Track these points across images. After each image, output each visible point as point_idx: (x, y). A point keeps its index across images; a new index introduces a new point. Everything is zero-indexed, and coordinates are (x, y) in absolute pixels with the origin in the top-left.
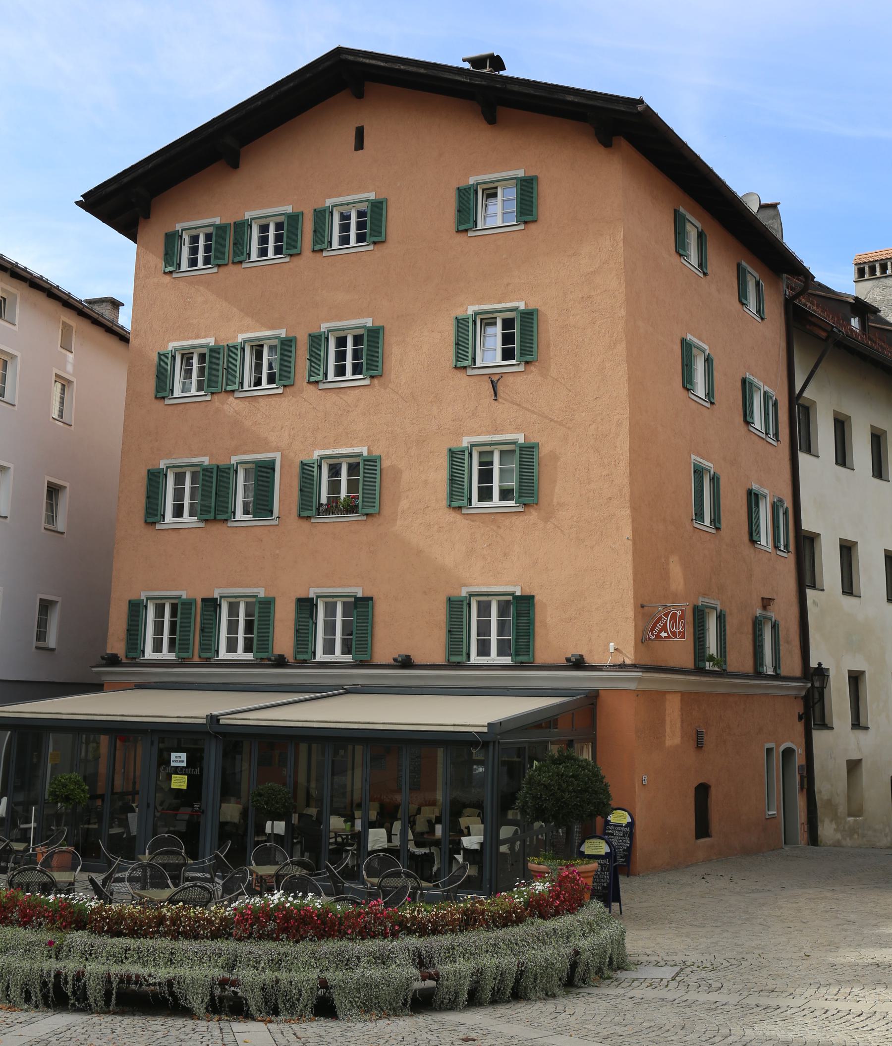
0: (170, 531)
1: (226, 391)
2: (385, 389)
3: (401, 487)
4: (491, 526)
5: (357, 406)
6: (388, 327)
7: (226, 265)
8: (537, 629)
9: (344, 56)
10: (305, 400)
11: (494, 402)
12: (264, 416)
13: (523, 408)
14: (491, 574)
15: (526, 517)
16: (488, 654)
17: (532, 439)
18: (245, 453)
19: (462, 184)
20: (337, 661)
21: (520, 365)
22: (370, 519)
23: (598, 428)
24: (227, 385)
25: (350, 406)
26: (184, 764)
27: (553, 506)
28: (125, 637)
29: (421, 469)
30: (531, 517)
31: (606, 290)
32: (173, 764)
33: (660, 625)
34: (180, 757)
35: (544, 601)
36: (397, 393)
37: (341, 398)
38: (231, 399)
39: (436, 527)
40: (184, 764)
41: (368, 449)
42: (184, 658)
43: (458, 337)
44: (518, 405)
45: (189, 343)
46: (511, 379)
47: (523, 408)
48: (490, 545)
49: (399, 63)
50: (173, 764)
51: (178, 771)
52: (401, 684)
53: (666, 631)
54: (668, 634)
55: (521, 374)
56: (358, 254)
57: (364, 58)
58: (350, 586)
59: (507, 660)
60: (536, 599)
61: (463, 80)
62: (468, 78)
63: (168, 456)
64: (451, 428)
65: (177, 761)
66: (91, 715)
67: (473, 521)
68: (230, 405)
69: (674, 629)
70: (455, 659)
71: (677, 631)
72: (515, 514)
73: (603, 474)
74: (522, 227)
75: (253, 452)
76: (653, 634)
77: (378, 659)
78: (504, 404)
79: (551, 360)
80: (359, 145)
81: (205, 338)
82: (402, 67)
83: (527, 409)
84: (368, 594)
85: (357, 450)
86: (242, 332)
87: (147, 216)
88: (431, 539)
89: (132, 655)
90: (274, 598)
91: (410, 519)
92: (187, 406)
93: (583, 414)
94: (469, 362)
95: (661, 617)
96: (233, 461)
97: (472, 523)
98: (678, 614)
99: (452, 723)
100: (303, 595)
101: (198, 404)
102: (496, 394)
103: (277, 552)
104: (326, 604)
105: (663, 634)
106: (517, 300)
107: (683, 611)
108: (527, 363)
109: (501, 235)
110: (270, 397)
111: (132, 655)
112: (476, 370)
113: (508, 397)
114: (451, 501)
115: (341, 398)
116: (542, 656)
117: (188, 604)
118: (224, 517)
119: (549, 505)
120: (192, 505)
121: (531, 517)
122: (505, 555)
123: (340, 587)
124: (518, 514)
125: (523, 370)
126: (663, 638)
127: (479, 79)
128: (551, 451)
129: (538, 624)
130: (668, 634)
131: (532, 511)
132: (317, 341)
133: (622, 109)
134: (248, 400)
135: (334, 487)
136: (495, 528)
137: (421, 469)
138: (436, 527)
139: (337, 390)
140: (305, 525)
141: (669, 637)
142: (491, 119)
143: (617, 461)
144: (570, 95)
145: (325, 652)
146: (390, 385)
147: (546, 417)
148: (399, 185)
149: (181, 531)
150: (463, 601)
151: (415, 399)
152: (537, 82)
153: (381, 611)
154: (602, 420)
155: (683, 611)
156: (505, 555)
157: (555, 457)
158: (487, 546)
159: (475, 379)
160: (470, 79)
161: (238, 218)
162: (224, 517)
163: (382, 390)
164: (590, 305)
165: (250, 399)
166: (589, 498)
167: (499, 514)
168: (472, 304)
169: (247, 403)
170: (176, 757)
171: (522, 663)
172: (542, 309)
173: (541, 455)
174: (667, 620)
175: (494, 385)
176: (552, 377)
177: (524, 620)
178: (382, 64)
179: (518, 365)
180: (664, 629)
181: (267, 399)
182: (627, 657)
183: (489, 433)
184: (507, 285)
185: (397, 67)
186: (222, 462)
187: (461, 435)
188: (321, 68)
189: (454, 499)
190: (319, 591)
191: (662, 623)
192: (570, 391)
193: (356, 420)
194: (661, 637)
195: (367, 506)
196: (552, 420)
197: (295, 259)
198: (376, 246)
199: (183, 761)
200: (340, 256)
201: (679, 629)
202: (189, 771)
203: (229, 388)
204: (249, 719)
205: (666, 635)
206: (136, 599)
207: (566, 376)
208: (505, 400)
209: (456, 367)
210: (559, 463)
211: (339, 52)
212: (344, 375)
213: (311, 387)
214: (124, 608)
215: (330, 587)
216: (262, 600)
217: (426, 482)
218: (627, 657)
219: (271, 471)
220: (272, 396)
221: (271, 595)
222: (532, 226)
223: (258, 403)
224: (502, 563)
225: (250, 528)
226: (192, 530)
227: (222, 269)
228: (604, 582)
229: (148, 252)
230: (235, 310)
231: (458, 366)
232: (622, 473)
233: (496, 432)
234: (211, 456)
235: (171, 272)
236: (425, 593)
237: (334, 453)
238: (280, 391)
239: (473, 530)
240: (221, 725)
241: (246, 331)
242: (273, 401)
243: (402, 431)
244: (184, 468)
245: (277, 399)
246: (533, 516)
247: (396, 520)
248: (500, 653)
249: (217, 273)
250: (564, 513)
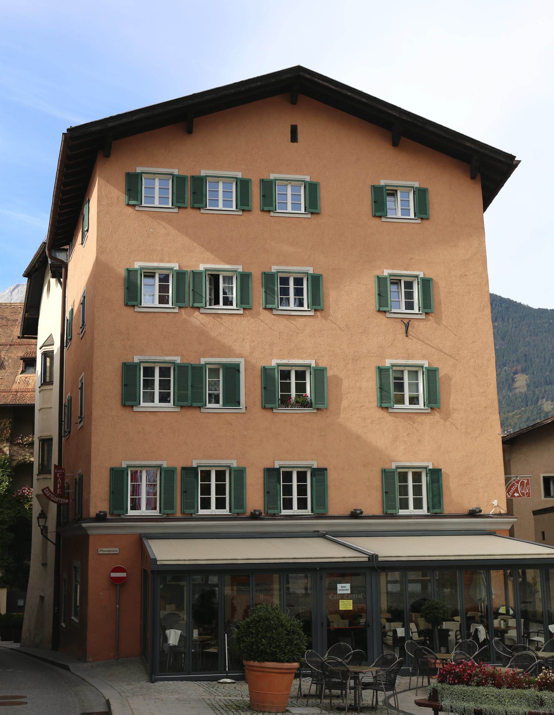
0: (147, 413)
1: (193, 307)
2: (326, 320)
3: (342, 391)
4: (409, 422)
5: (304, 330)
6: (325, 276)
7: (186, 208)
8: (444, 491)
9: (302, 73)
10: (262, 321)
11: (405, 337)
12: (228, 330)
13: (425, 343)
14: (411, 454)
15: (432, 417)
17: (433, 365)
18: (212, 356)
20: (299, 514)
21: (422, 315)
22: (319, 412)
23: (475, 361)
24: (194, 302)
25: (299, 329)
26: (349, 592)
27: (450, 410)
28: (108, 497)
29: (357, 379)
30: (435, 417)
31: (476, 273)
32: (339, 592)
33: (513, 489)
34: (345, 587)
35: (448, 472)
36: (335, 324)
37: (291, 323)
38: (197, 313)
39: (370, 420)
40: (349, 592)
41: (315, 361)
42: (168, 514)
43: (379, 290)
44: (423, 341)
45: (155, 264)
46: (416, 323)
47: (425, 343)
48: (408, 434)
49: (346, 90)
50: (339, 592)
51: (344, 597)
52: (150, 532)
53: (518, 493)
54: (519, 494)
55: (423, 320)
56: (298, 219)
57: (318, 79)
58: (307, 460)
60: (442, 471)
61: (394, 114)
62: (398, 113)
63: (141, 353)
64: (377, 352)
65: (343, 590)
66: (265, 559)
67: (396, 417)
68: (196, 318)
69: (523, 491)
70: (390, 511)
71: (525, 492)
72: (425, 414)
73: (481, 391)
74: (176, 210)
75: (219, 356)
77: (332, 512)
78: (412, 339)
79: (443, 314)
80: (294, 138)
81: (169, 262)
82: (349, 94)
83: (428, 345)
84: (322, 466)
85: (307, 362)
86: (203, 263)
87: (107, 155)
88: (366, 428)
89: (116, 512)
90: (245, 468)
91: (350, 414)
92: (156, 315)
93: (465, 352)
94: (203, 305)
95: (514, 484)
97: (396, 419)
98: (525, 482)
99: (342, 556)
100: (270, 466)
101: (166, 314)
102: (406, 333)
103: (245, 433)
105: (516, 494)
106: (418, 270)
107: (528, 480)
108: (426, 313)
109: (404, 224)
110: (231, 316)
111: (116, 512)
113: (415, 335)
114: (382, 403)
115: (291, 323)
116: (447, 509)
118: (199, 404)
119: (447, 409)
121: (435, 417)
122: (419, 441)
123: (299, 460)
124: (427, 414)
125: (424, 318)
127: (406, 116)
128: (446, 374)
129: (444, 488)
130: (519, 494)
131: (436, 413)
132: (268, 278)
133: (502, 159)
134: (212, 315)
135: (301, 388)
136: (411, 423)
137: (357, 379)
138: (370, 420)
139: (288, 317)
140: (268, 414)
141: (520, 496)
142: (395, 144)
143: (489, 384)
144: (469, 142)
145: (415, 508)
146: (329, 318)
147: (441, 351)
148: (327, 174)
149: (158, 414)
150: (394, 472)
151: (349, 330)
152: (442, 126)
153: (332, 477)
154: (478, 356)
155: (528, 480)
156: (419, 441)
157: (448, 378)
158: (407, 435)
159: (391, 321)
160: (399, 115)
161: (195, 174)
162: (199, 404)
163: (324, 321)
164: (466, 280)
165: (214, 315)
166: (472, 406)
167: (413, 414)
168: (387, 268)
169: (212, 319)
170: (342, 587)
171: (436, 513)
172: (435, 278)
173: (440, 376)
174: (518, 486)
175: (407, 326)
176: (443, 325)
177: (436, 485)
178: (333, 87)
180: (516, 491)
181: (229, 317)
182: (502, 509)
183: (404, 358)
184: (411, 259)
185: (345, 93)
186: (192, 360)
187: (385, 358)
188: (283, 78)
189: (383, 401)
191: (515, 487)
192: (456, 335)
193: (304, 340)
194: (515, 496)
195: (319, 402)
196: (445, 353)
197: (246, 214)
198: (313, 216)
199: (348, 590)
200: (284, 218)
201: (526, 491)
202: (355, 596)
203: (196, 305)
204: (402, 557)
205: (518, 495)
206: (117, 466)
207: (453, 325)
208: (413, 337)
209: (379, 311)
210: (452, 382)
211: (299, 69)
212: (413, 309)
213: (266, 312)
214: (106, 475)
215: (290, 460)
216: (236, 469)
217: (360, 388)
218: (502, 509)
219: (237, 372)
220: (234, 315)
221: (242, 465)
222: (425, 222)
223: (222, 319)
224: (418, 447)
226: (168, 413)
227: (181, 210)
228: (485, 461)
229: (109, 185)
230: (195, 244)
231: (381, 310)
232: (493, 391)
233: (409, 358)
234: (182, 356)
235: (134, 206)
236: (364, 466)
237: (288, 362)
238: (241, 312)
239: (396, 424)
240: (379, 561)
241: (207, 262)
242: (235, 319)
243: (341, 351)
245: (238, 318)
246: (437, 416)
247: (340, 414)
249: (177, 213)
250: (457, 415)
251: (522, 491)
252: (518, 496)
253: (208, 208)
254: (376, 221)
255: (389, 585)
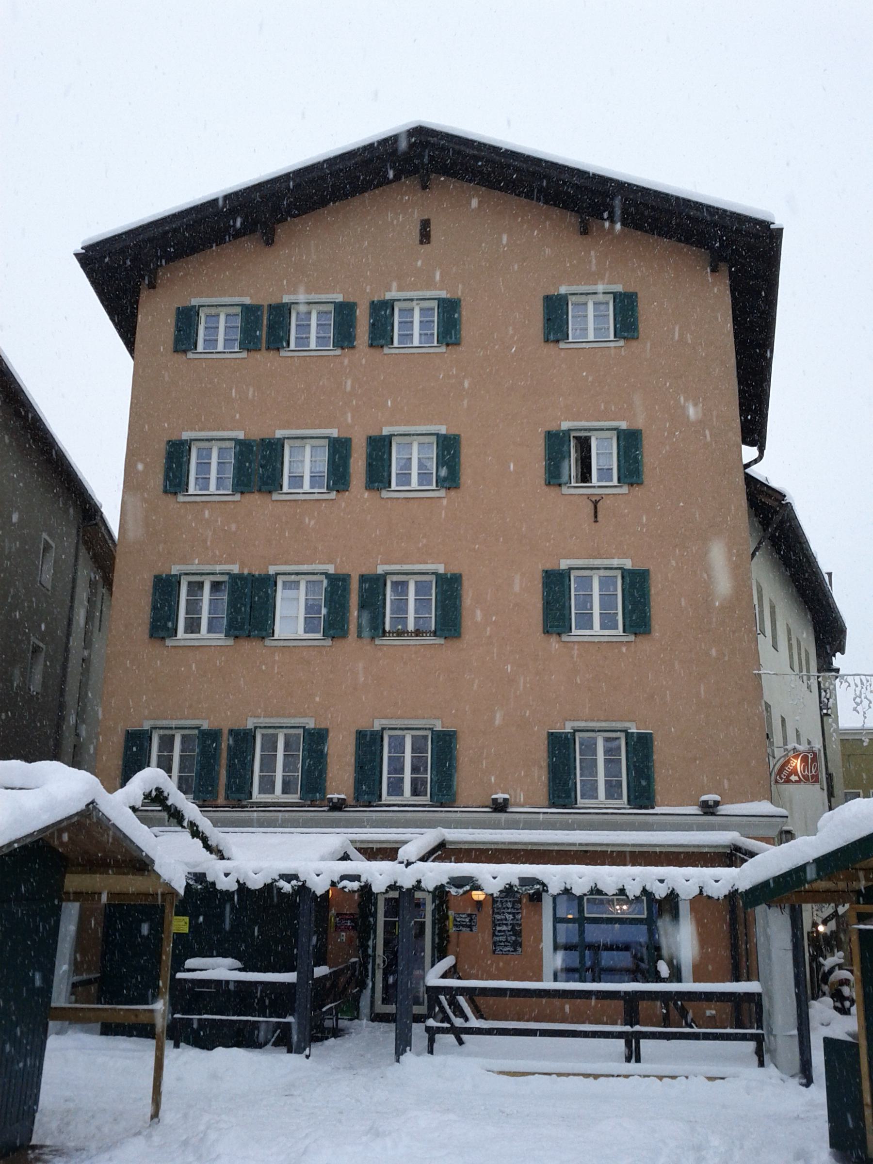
16: (273, 792)
18: (286, 563)
19: (552, 291)
54: (799, 777)
59: (294, 798)
63: (184, 561)
69: (806, 772)
71: (810, 774)
76: (781, 779)
80: (425, 236)
96: (174, 571)
98: (810, 757)
102: (596, 517)
104: (161, 738)
112: (284, 495)
117: (212, 735)
120: (211, 621)
125: (627, 492)
126: (793, 782)
130: (799, 777)
161: (274, 301)
175: (595, 504)
179: (234, 495)
190: (385, 722)
201: (811, 772)
205: (796, 778)
225: (207, 648)
234: (242, 565)
244: (299, 576)
248: (285, 791)
251: (804, 772)
252: (796, 782)
253: (570, 340)
254: (551, 348)
255: (561, 927)
